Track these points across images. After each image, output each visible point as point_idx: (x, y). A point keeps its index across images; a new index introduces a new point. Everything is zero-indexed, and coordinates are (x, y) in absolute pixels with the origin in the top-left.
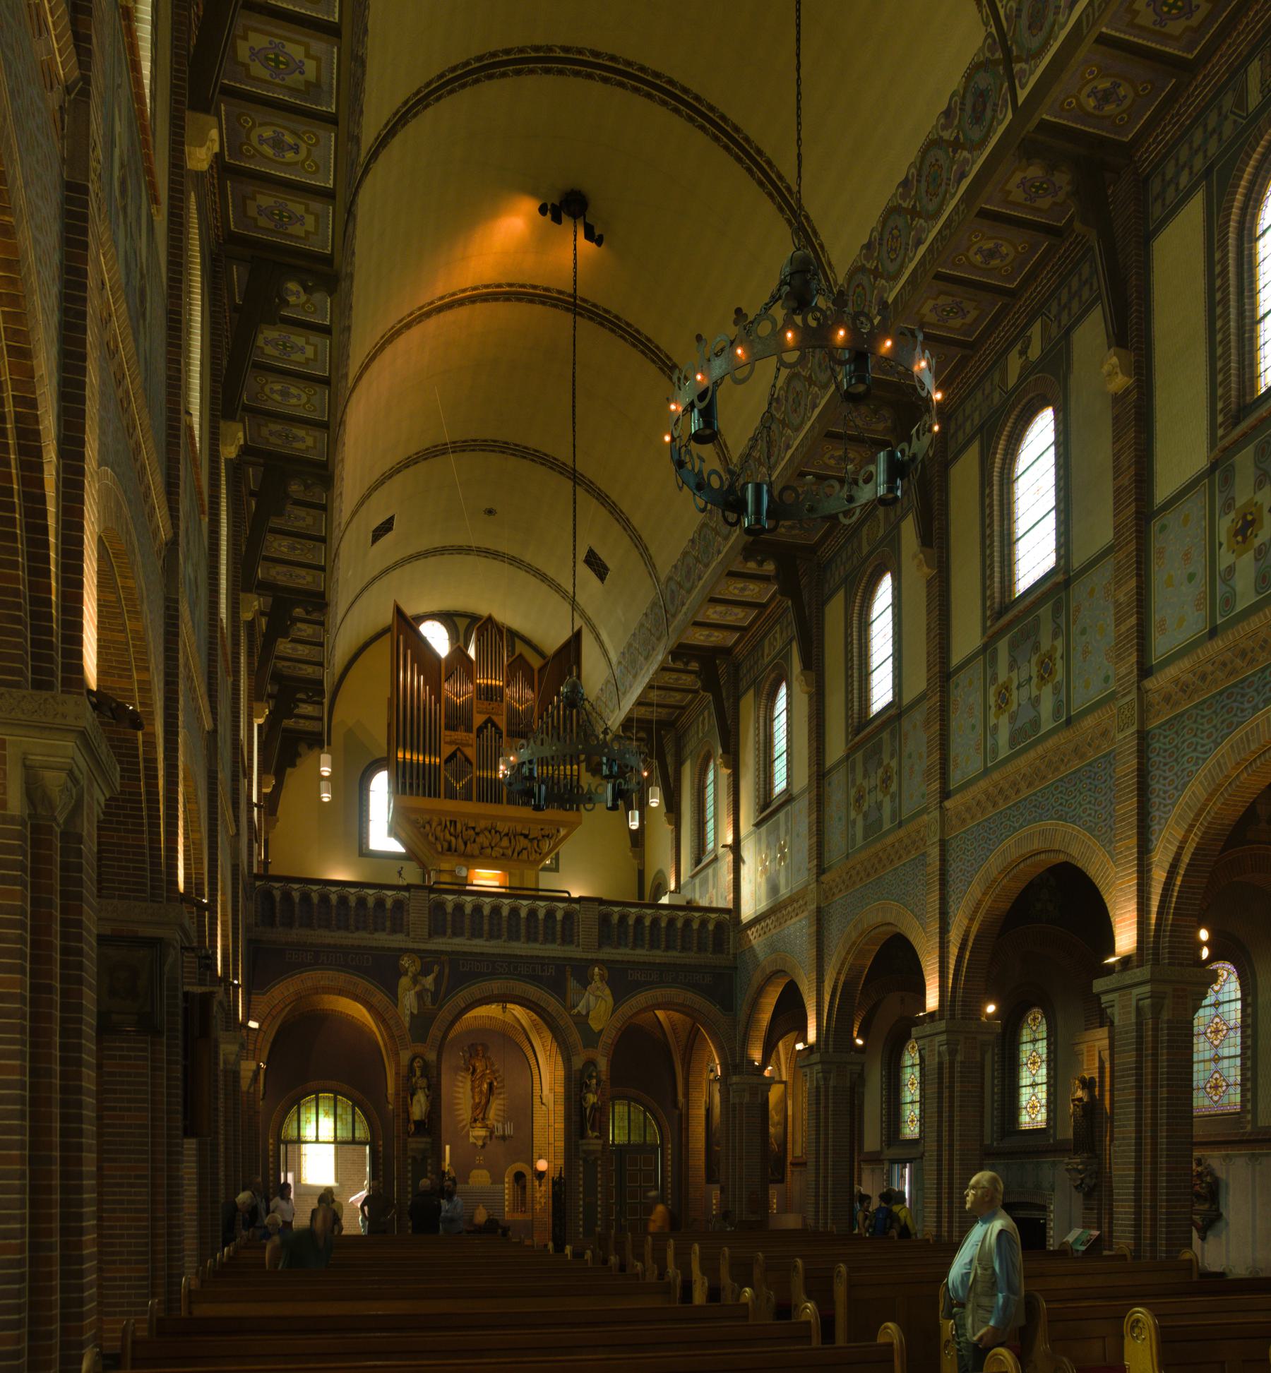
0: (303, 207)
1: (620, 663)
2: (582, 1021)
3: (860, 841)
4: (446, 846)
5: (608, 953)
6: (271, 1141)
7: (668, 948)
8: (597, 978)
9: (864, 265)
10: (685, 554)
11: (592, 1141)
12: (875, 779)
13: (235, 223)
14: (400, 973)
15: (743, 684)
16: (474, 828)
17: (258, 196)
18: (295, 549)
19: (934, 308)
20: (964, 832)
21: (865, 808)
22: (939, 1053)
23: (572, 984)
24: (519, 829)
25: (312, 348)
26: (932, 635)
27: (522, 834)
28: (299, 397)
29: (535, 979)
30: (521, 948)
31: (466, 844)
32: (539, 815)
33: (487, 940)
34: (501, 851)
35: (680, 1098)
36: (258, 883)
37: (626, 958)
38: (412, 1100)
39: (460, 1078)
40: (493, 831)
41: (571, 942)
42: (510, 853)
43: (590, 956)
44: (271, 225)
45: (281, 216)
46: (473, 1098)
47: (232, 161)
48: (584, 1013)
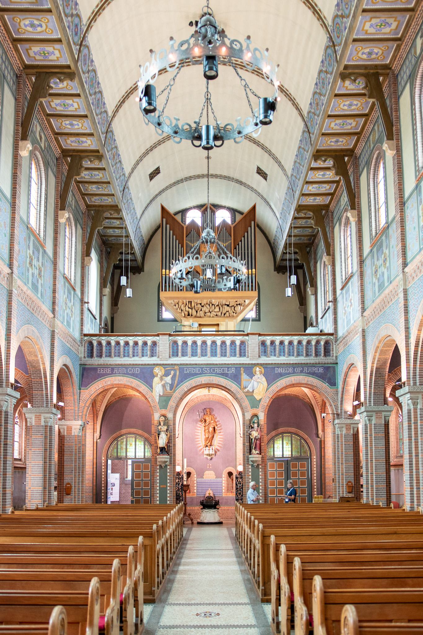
0: (52, 48)
1: (281, 218)
2: (250, 395)
3: (377, 294)
4: (187, 313)
5: (264, 360)
6: (103, 458)
7: (298, 355)
8: (258, 373)
9: (337, 14)
10: (295, 162)
12: (381, 261)
13: (27, 61)
14: (153, 376)
15: (335, 221)
16: (201, 304)
17: (32, 48)
18: (99, 188)
19: (371, 26)
20: (414, 284)
21: (378, 276)
22: (408, 405)
23: (244, 377)
24: (224, 302)
25: (76, 103)
26: (396, 184)
27: (226, 305)
28: (78, 125)
29: (134, 375)
30: (218, 360)
31: (197, 312)
32: (197, 295)
33: (278, 357)
34: (215, 314)
35: (320, 432)
36: (86, 338)
37: (274, 362)
38: (158, 437)
39: (199, 426)
40: (211, 305)
41: (245, 356)
42: (220, 315)
43: (254, 362)
44: (42, 58)
45: (44, 53)
46: (205, 435)
47: (17, 37)
48: (251, 391)
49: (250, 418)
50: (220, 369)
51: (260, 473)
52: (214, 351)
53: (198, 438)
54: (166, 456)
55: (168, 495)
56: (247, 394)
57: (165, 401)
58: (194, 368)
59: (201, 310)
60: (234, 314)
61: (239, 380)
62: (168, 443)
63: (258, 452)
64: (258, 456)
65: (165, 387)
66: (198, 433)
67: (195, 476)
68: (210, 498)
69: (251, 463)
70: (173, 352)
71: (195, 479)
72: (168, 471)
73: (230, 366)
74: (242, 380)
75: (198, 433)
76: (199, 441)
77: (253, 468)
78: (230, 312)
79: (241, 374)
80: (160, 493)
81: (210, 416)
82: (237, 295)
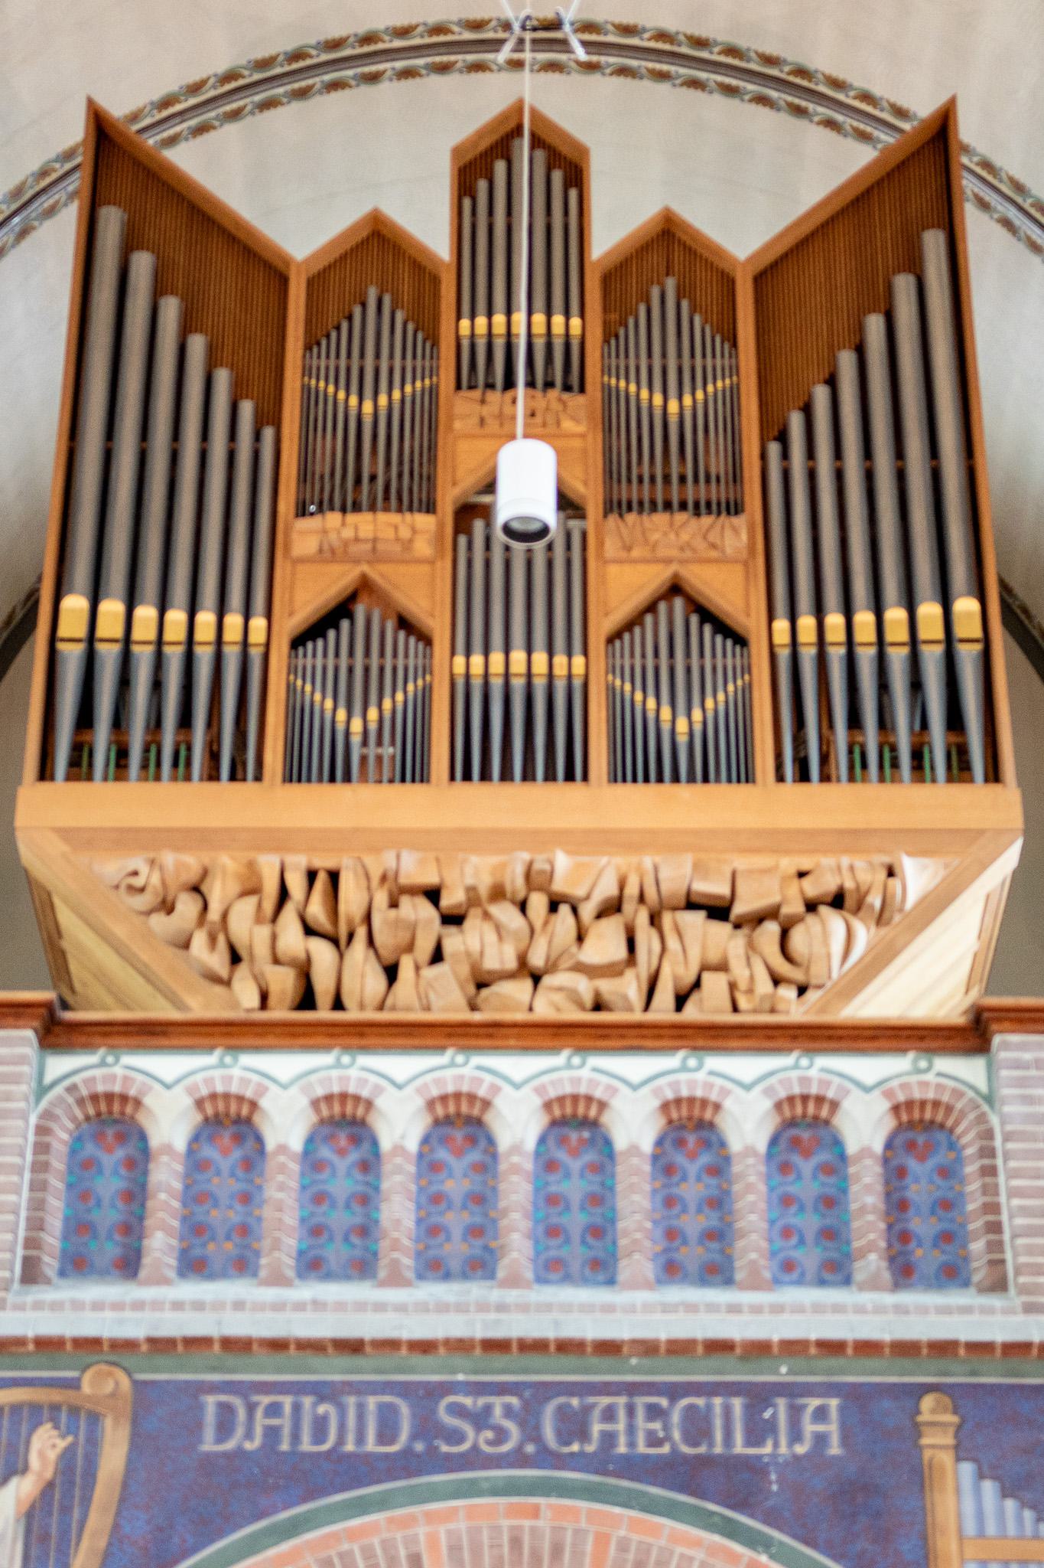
4: (282, 982)
16: (433, 895)
31: (391, 972)
40: (538, 903)
50: (654, 1412)
52: (576, 1220)
58: (323, 1392)
59: (437, 957)
60: (788, 993)
70: (79, 1227)
73: (783, 1373)
78: (739, 972)
79: (919, 1477)
82: (806, 821)
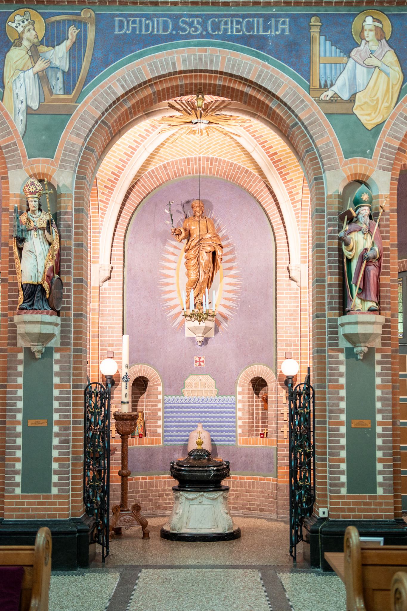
8: (370, 35)
11: (361, 318)
38: (20, 250)
39: (171, 249)
46: (188, 275)
48: (346, 96)
49: (341, 190)
50: (238, 23)
51: (378, 381)
53: (168, 284)
54: (47, 318)
55: (55, 454)
56: (333, 108)
57: (48, 128)
58: (148, 17)
61: (305, 60)
62: (52, 269)
63: (373, 305)
64: (373, 317)
65: (48, 82)
66: (169, 268)
67: (160, 389)
68: (200, 457)
69: (344, 344)
71: (160, 397)
72: (56, 368)
73: (274, 11)
74: (316, 59)
75: (169, 268)
76: (172, 299)
77: (353, 360)
79: (309, 40)
80: (25, 448)
81: (203, 221)
